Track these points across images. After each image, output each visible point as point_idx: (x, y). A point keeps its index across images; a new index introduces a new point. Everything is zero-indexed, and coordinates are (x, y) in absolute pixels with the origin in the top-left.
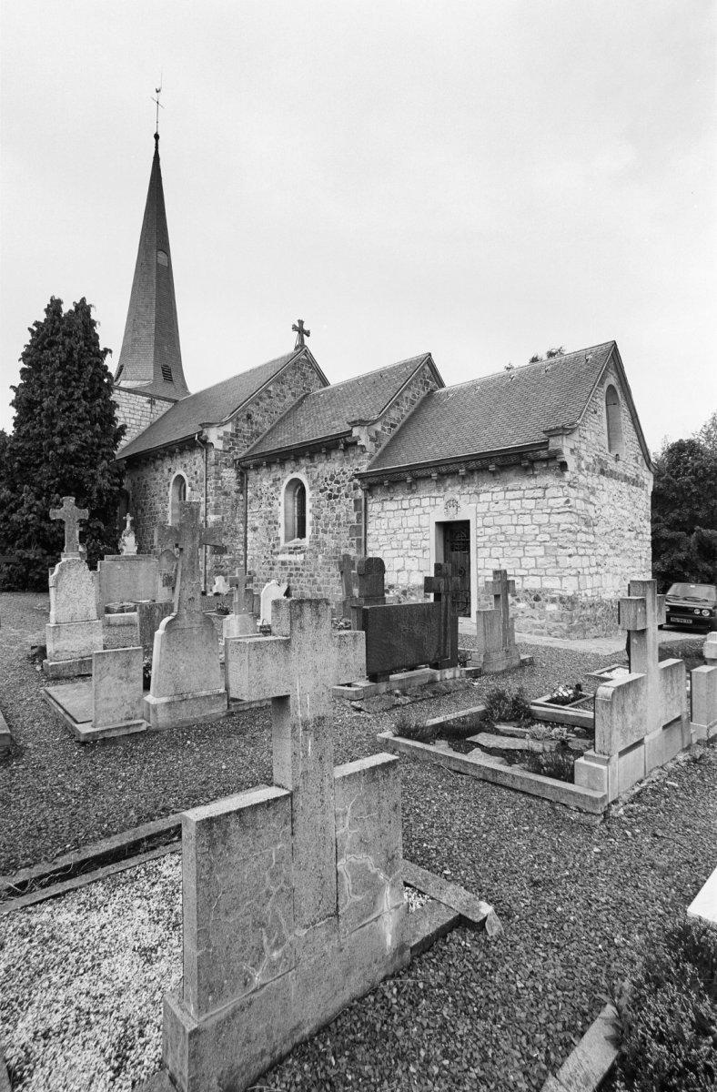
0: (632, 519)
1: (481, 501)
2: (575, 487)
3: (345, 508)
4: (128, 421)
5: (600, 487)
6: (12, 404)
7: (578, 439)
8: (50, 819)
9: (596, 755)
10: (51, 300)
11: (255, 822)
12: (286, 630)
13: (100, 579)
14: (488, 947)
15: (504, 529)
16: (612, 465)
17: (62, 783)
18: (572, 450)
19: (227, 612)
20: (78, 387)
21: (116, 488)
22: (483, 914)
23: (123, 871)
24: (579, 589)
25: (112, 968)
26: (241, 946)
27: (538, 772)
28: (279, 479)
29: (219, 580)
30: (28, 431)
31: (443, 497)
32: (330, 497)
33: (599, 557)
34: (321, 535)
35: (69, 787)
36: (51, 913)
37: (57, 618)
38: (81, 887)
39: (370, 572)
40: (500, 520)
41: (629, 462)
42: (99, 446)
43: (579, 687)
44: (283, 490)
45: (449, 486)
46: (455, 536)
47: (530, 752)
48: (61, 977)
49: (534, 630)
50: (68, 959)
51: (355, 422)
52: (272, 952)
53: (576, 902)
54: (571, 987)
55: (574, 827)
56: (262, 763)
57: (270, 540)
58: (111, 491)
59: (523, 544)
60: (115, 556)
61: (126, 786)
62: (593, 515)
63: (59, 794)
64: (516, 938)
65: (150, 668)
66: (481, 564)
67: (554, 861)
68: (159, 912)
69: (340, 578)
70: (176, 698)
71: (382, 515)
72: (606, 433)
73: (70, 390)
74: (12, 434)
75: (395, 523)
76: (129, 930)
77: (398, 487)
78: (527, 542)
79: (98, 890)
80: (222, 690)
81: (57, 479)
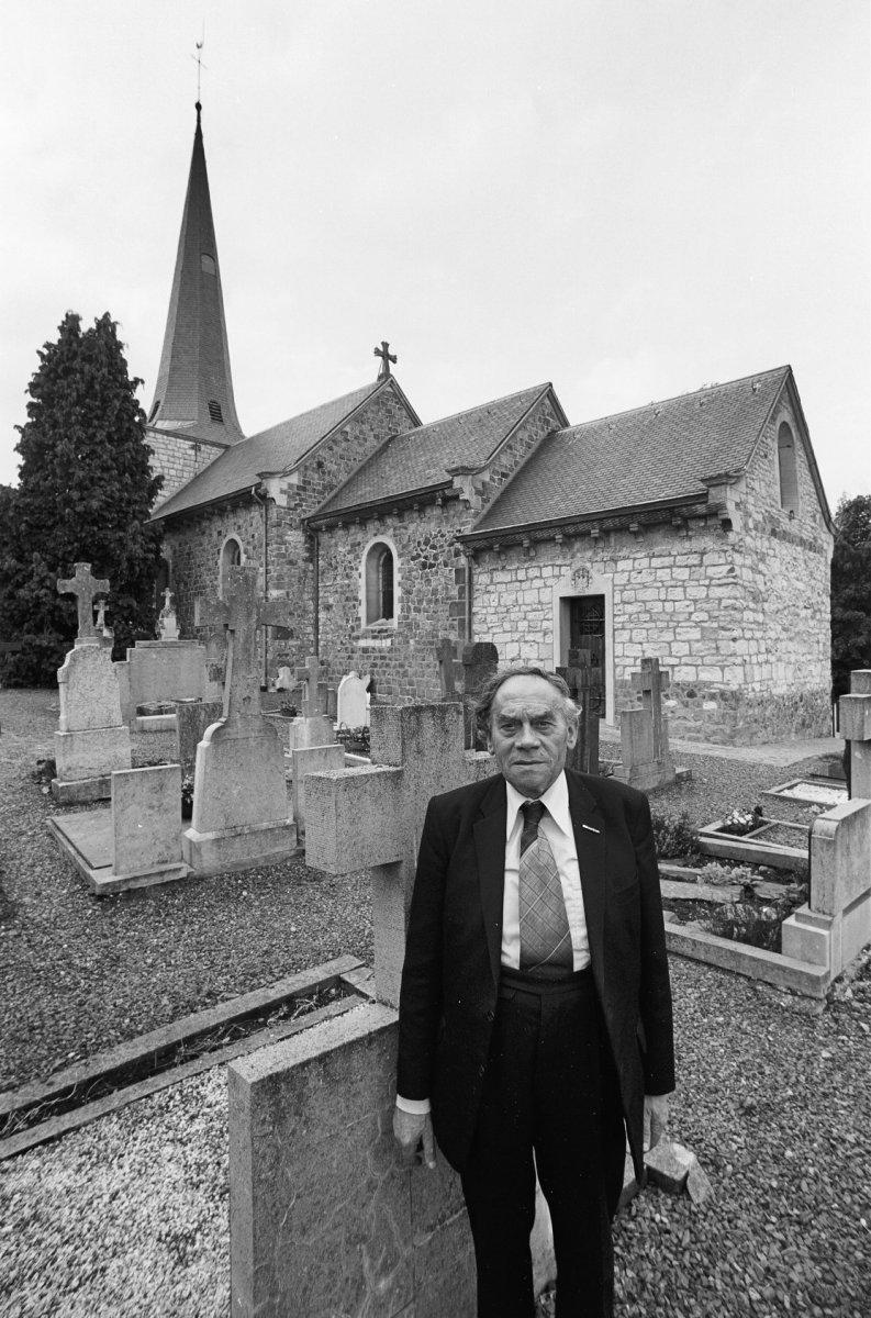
0: (809, 593)
1: (619, 569)
2: (741, 552)
3: (443, 580)
4: (166, 471)
5: (771, 552)
6: (16, 449)
7: (744, 489)
8: (47, 1012)
9: (813, 915)
10: (67, 315)
11: (349, 1071)
12: (396, 755)
13: (129, 672)
14: (694, 1222)
15: (649, 605)
16: (785, 524)
17: (69, 956)
18: (737, 504)
19: (294, 713)
20: (101, 427)
21: (151, 556)
22: (684, 1167)
23: (148, 1096)
24: (746, 683)
25: (124, 1275)
26: (328, 1281)
27: (727, 935)
28: (359, 544)
29: (284, 672)
30: (38, 483)
31: (570, 565)
32: (424, 566)
33: (769, 642)
35: (78, 962)
36: (38, 1170)
37: (68, 725)
38: (85, 1125)
39: (478, 661)
40: (642, 595)
41: (806, 523)
42: (129, 503)
43: (758, 811)
44: (364, 558)
45: (578, 551)
46: (584, 616)
47: (711, 904)
48: (42, 1297)
49: (687, 735)
50: (56, 1259)
51: (456, 470)
52: (377, 1281)
53: (812, 1141)
54: (833, 1301)
55: (787, 1017)
56: (345, 923)
57: (348, 621)
58: (145, 560)
59: (672, 622)
60: (148, 642)
61: (160, 958)
62: (762, 588)
63: (62, 973)
64: (733, 1206)
65: (192, 791)
66: (619, 651)
67: (767, 1072)
68: (201, 1167)
69: (437, 669)
70: (227, 833)
71: (491, 588)
72: (779, 483)
73: (91, 431)
74: (18, 488)
75: (508, 599)
76: (154, 1202)
77: (511, 553)
78: (679, 622)
79: (111, 1128)
80: (289, 821)
81: (76, 544)
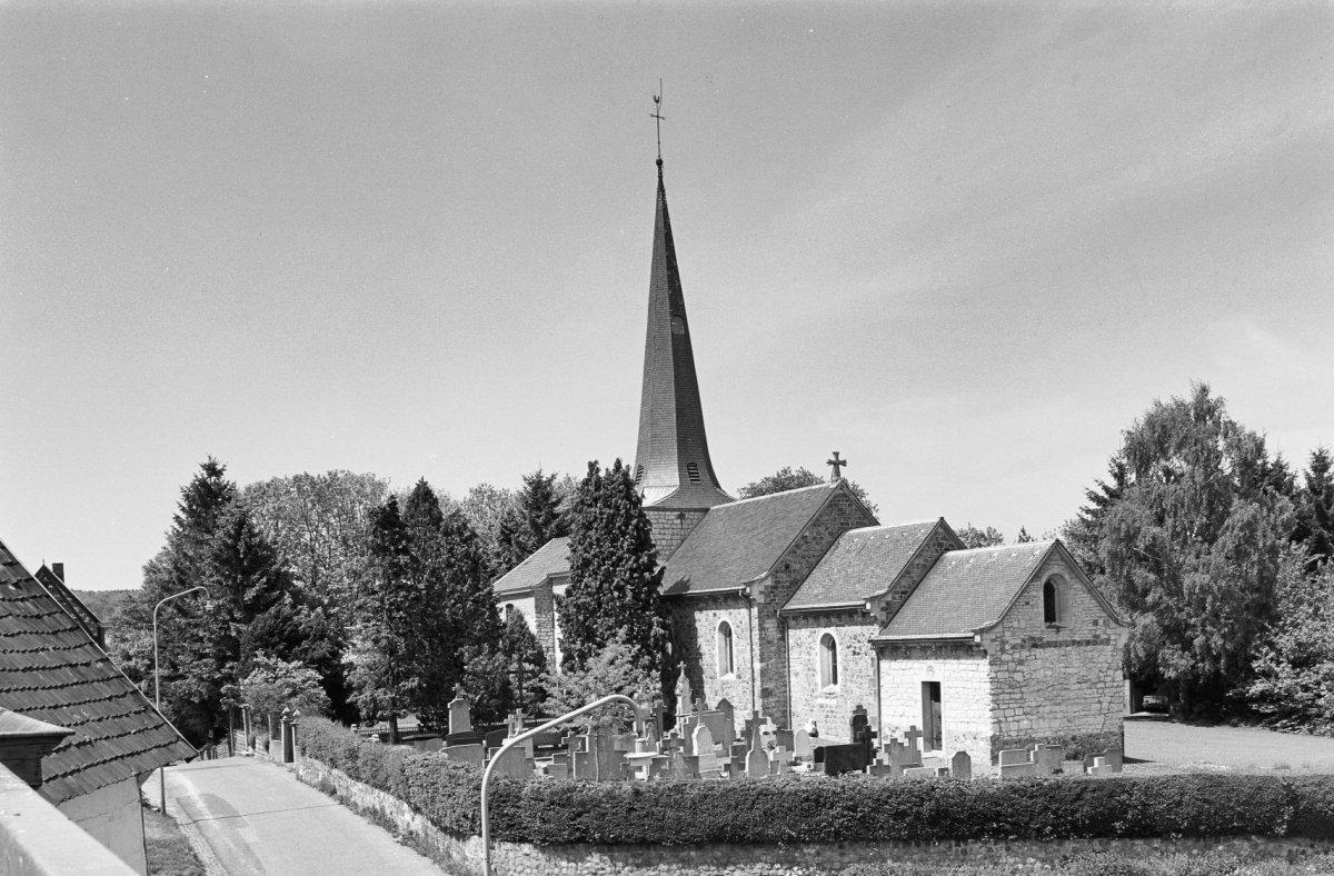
32: (854, 653)
34: (849, 684)
46: (933, 691)
